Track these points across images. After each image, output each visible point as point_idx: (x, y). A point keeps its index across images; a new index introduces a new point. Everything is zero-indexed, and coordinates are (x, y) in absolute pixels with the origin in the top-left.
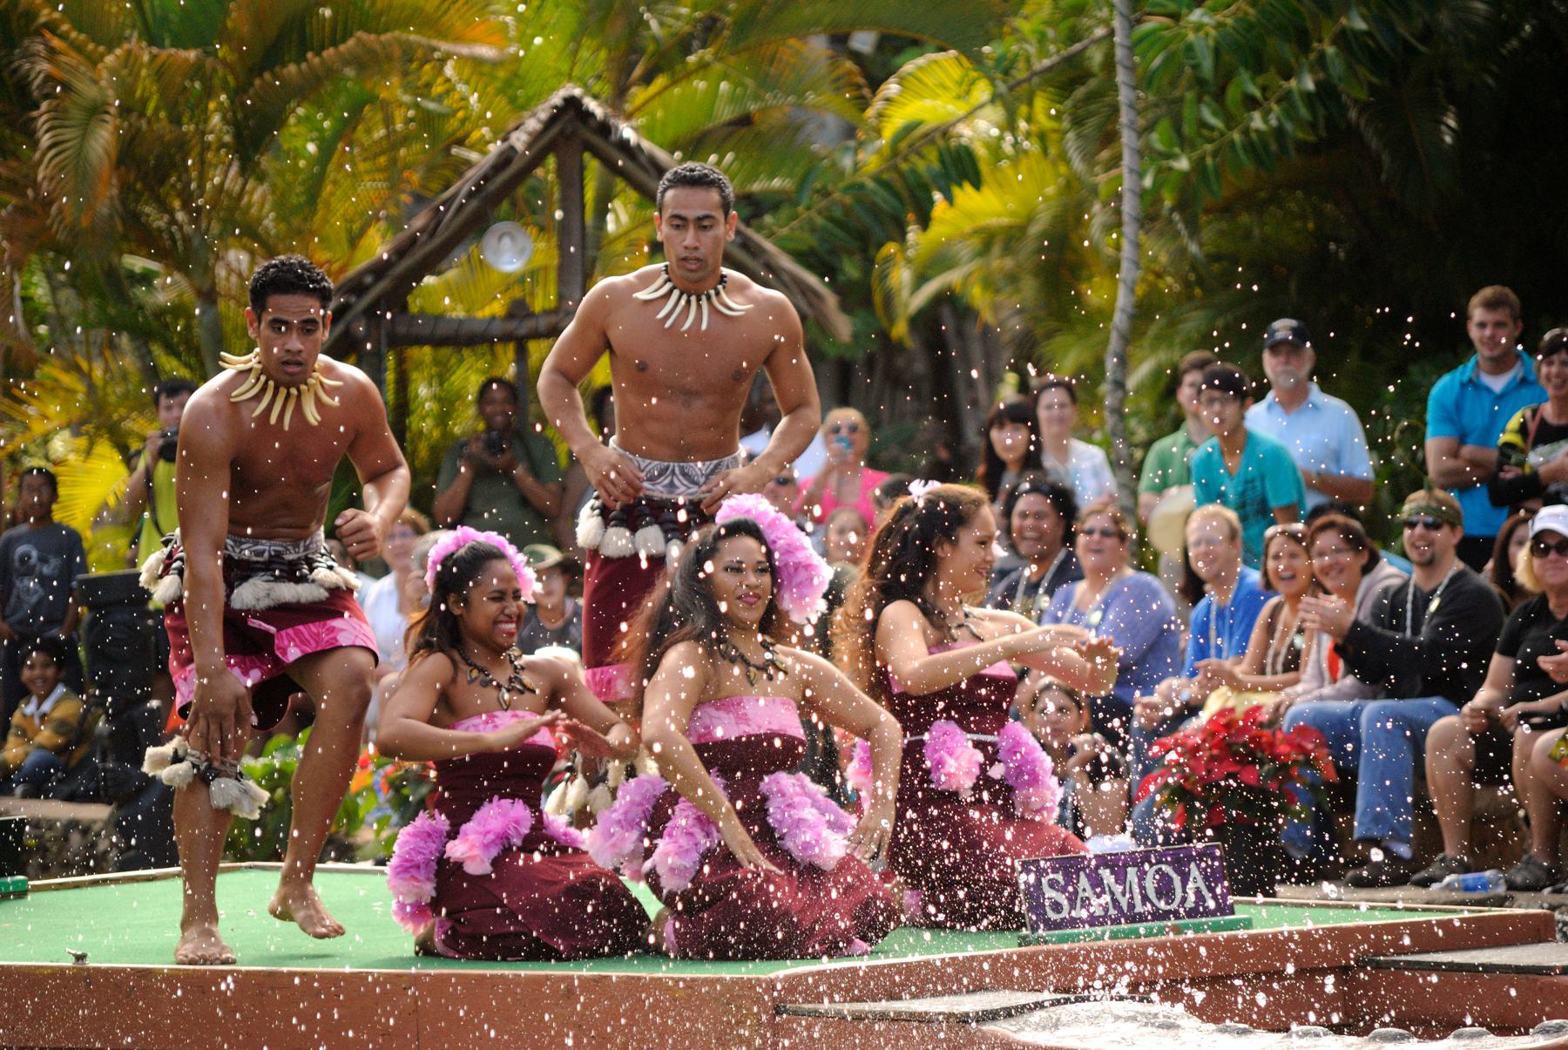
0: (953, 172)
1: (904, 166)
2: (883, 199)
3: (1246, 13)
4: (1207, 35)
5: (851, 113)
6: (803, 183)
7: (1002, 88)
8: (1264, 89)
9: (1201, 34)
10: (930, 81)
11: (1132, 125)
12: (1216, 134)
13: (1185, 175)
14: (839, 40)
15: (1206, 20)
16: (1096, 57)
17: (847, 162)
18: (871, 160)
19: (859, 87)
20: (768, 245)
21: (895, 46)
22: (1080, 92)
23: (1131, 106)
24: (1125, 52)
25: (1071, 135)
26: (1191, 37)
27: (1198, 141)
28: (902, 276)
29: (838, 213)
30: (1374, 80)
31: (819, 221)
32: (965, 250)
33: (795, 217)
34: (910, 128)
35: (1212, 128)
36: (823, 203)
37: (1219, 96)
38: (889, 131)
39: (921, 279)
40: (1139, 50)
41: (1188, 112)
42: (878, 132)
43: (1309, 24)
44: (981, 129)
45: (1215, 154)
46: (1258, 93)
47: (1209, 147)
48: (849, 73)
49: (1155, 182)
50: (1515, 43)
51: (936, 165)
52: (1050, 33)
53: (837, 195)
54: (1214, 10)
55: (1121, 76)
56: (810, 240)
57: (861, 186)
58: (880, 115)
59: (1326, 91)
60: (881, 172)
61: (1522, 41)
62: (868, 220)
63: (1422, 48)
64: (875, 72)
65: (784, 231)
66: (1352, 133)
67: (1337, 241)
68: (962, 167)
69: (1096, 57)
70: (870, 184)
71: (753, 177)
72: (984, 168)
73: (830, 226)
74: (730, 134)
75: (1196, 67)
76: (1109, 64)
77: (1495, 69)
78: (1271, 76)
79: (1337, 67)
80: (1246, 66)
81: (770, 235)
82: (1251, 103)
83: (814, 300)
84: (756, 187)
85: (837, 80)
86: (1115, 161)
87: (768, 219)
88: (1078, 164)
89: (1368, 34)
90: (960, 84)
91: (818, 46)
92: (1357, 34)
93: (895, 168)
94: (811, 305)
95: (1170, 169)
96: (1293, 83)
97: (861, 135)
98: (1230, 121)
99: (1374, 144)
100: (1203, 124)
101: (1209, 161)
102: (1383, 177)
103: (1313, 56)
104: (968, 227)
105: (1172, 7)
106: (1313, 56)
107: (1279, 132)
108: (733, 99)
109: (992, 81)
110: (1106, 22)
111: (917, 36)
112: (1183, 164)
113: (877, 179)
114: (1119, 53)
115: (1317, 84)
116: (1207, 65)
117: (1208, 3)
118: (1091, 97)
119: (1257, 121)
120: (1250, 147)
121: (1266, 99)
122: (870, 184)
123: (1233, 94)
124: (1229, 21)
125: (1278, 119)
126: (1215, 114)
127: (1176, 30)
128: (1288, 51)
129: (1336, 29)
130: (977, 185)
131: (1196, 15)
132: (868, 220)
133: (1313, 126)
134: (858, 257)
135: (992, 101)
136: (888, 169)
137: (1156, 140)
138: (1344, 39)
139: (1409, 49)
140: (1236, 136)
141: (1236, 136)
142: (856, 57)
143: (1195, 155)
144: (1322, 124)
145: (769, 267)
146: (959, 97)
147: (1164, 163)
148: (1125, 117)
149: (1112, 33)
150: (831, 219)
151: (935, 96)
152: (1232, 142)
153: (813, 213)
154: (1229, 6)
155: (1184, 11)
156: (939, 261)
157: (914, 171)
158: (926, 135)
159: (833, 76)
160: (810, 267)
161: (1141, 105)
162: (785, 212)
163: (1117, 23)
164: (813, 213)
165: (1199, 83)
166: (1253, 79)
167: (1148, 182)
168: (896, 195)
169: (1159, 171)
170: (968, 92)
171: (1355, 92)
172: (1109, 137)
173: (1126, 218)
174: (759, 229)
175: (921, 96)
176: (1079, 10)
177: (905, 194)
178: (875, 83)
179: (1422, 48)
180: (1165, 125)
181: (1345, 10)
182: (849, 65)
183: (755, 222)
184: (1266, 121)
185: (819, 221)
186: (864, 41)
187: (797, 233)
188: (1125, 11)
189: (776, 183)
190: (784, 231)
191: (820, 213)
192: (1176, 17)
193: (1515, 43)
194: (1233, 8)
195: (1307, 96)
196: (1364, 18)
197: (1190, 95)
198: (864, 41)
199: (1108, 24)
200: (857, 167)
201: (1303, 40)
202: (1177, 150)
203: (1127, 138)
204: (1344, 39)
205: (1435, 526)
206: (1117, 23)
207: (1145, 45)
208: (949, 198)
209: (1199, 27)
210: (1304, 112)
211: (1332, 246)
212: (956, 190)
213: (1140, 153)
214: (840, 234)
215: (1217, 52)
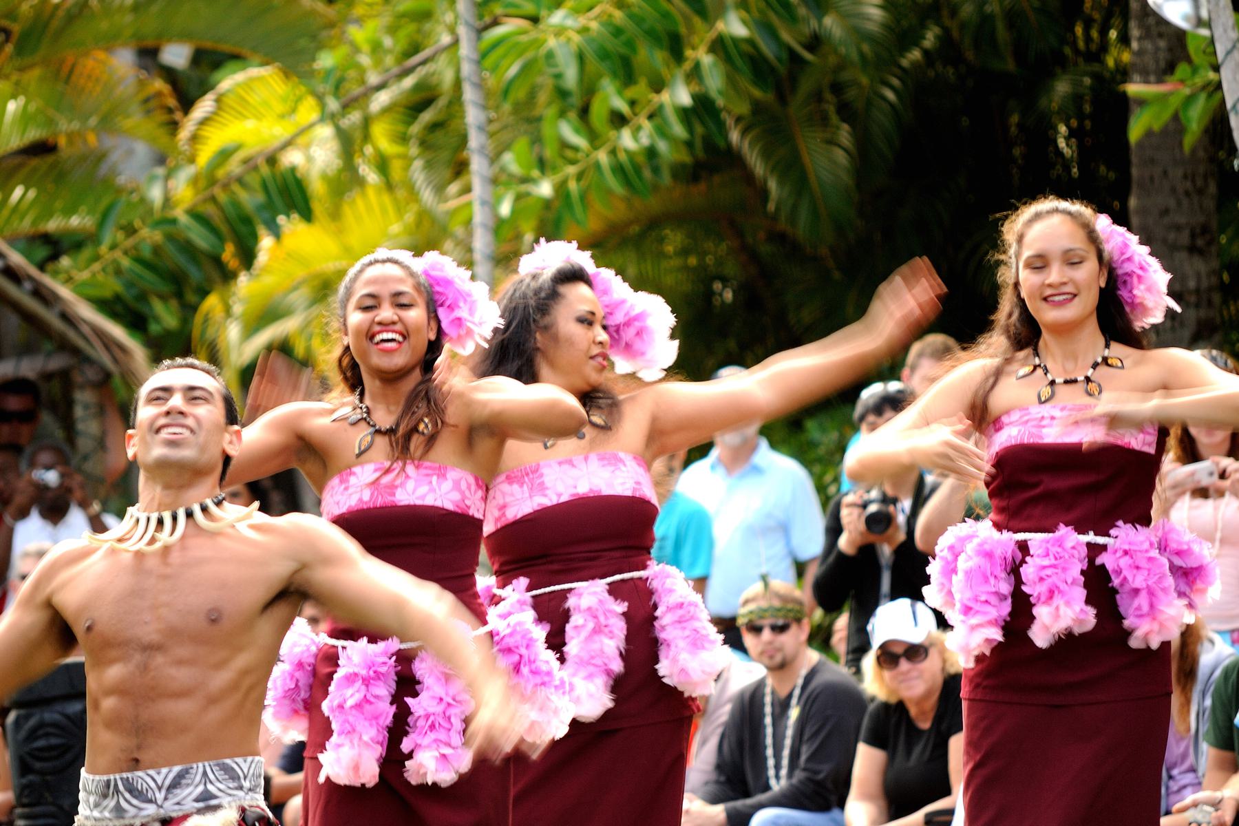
0: (278, 201)
1: (222, 197)
2: (200, 238)
3: (610, 16)
4: (569, 40)
5: (162, 135)
6: (101, 224)
7: (333, 105)
8: (632, 103)
9: (562, 39)
10: (253, 99)
11: (482, 150)
12: (580, 155)
13: (547, 204)
14: (148, 55)
15: (570, 22)
16: (448, 78)
17: (156, 194)
18: (183, 190)
19: (170, 111)
20: (64, 292)
21: (210, 61)
22: (427, 116)
23: (481, 128)
24: (474, 67)
25: (418, 164)
26: (552, 42)
27: (559, 162)
28: (233, 332)
29: (147, 253)
30: (757, 93)
31: (126, 262)
32: (299, 297)
33: (97, 258)
34: (224, 155)
35: (576, 149)
36: (130, 242)
37: (584, 112)
38: (205, 156)
39: (252, 329)
40: (489, 62)
41: (547, 130)
42: (192, 160)
43: (683, 30)
44: (316, 156)
45: (580, 177)
46: (623, 107)
47: (571, 170)
48: (159, 94)
49: (514, 211)
50: (916, 55)
51: (260, 198)
52: (388, 42)
53: (145, 232)
54: (576, 11)
55: (469, 94)
56: (112, 286)
57: (174, 221)
58: (194, 138)
59: (703, 109)
60: (195, 205)
61: (926, 53)
62: (180, 260)
63: (807, 56)
64: (185, 91)
65: (84, 275)
66: (732, 158)
67: (725, 280)
68: (290, 196)
69: (448, 78)
70: (183, 219)
71: (48, 214)
72: (318, 208)
73: (139, 269)
74: (20, 166)
75: (558, 76)
76: (458, 84)
77: (895, 82)
78: (640, 89)
79: (714, 82)
80: (615, 75)
81: (69, 280)
82: (619, 120)
83: (119, 355)
84: (52, 225)
85: (146, 101)
86: (467, 190)
87: (65, 262)
88: (427, 196)
89: (750, 41)
90: (284, 99)
91: (123, 62)
92: (736, 41)
93: (213, 199)
94: (116, 360)
95: (528, 194)
96: (665, 97)
97: (171, 162)
98: (594, 138)
99: (757, 165)
100: (565, 145)
101: (573, 186)
102: (771, 206)
103: (687, 66)
104: (300, 273)
105: (530, 8)
106: (687, 66)
107: (651, 152)
108: (25, 118)
109: (320, 98)
110: (452, 30)
111: (236, 50)
112: (545, 189)
113: (194, 214)
114: (467, 69)
115: (695, 97)
116: (571, 76)
117: (569, 4)
118: (435, 126)
119: (626, 140)
120: (619, 170)
121: (635, 114)
122: (183, 219)
123: (598, 112)
124: (594, 25)
125: (651, 136)
126: (577, 131)
127: (533, 34)
128: (657, 58)
129: (712, 35)
130: (307, 215)
131: (558, 18)
132: (180, 260)
133: (689, 144)
134: (174, 303)
135: (322, 120)
136: (205, 201)
137: (511, 161)
138: (720, 46)
139: (794, 57)
140: (602, 157)
141: (602, 157)
142: (170, 74)
143: (558, 177)
144: (698, 143)
145: (101, 339)
146: (282, 117)
147: (524, 188)
148: (475, 140)
149: (456, 42)
150: (139, 260)
151: (259, 117)
152: (597, 166)
153: (118, 254)
154: (591, 9)
155: (543, 13)
156: (268, 314)
157: (236, 204)
158: (246, 161)
159: (142, 96)
160: (114, 315)
161: (493, 127)
162: (87, 253)
163: (462, 31)
164: (118, 254)
165: (562, 94)
166: (620, 93)
167: (505, 209)
168: (214, 230)
169: (519, 198)
170: (294, 110)
171: (733, 107)
172: (460, 168)
173: (478, 256)
174: (55, 274)
175: (242, 116)
176: (424, 15)
177: (224, 228)
178: (187, 104)
179: (807, 56)
180: (522, 144)
181: (721, 11)
182: (159, 85)
183: (50, 267)
184: (635, 137)
185: (126, 262)
186: (176, 55)
187: (100, 277)
188: (471, 20)
189: (75, 221)
190: (84, 275)
191: (126, 253)
192: (535, 20)
193: (916, 55)
194: (597, 11)
195: (685, 114)
196: (745, 22)
197: (550, 112)
198: (176, 55)
199: (453, 28)
200: (167, 202)
201: (675, 47)
202: (535, 173)
203: (477, 165)
204: (720, 46)
205: (780, 629)
206: (462, 31)
207: (500, 51)
208: (276, 232)
209: (559, 31)
210: (679, 130)
211: (717, 286)
212: (281, 219)
213: (494, 182)
214: (149, 276)
215: (581, 58)
